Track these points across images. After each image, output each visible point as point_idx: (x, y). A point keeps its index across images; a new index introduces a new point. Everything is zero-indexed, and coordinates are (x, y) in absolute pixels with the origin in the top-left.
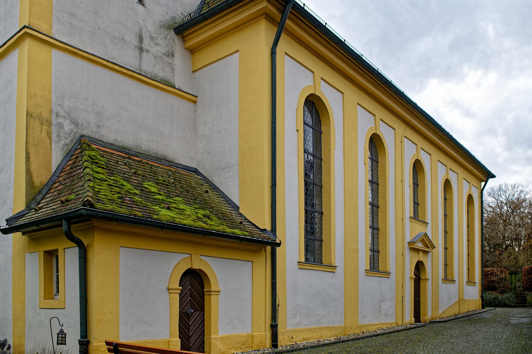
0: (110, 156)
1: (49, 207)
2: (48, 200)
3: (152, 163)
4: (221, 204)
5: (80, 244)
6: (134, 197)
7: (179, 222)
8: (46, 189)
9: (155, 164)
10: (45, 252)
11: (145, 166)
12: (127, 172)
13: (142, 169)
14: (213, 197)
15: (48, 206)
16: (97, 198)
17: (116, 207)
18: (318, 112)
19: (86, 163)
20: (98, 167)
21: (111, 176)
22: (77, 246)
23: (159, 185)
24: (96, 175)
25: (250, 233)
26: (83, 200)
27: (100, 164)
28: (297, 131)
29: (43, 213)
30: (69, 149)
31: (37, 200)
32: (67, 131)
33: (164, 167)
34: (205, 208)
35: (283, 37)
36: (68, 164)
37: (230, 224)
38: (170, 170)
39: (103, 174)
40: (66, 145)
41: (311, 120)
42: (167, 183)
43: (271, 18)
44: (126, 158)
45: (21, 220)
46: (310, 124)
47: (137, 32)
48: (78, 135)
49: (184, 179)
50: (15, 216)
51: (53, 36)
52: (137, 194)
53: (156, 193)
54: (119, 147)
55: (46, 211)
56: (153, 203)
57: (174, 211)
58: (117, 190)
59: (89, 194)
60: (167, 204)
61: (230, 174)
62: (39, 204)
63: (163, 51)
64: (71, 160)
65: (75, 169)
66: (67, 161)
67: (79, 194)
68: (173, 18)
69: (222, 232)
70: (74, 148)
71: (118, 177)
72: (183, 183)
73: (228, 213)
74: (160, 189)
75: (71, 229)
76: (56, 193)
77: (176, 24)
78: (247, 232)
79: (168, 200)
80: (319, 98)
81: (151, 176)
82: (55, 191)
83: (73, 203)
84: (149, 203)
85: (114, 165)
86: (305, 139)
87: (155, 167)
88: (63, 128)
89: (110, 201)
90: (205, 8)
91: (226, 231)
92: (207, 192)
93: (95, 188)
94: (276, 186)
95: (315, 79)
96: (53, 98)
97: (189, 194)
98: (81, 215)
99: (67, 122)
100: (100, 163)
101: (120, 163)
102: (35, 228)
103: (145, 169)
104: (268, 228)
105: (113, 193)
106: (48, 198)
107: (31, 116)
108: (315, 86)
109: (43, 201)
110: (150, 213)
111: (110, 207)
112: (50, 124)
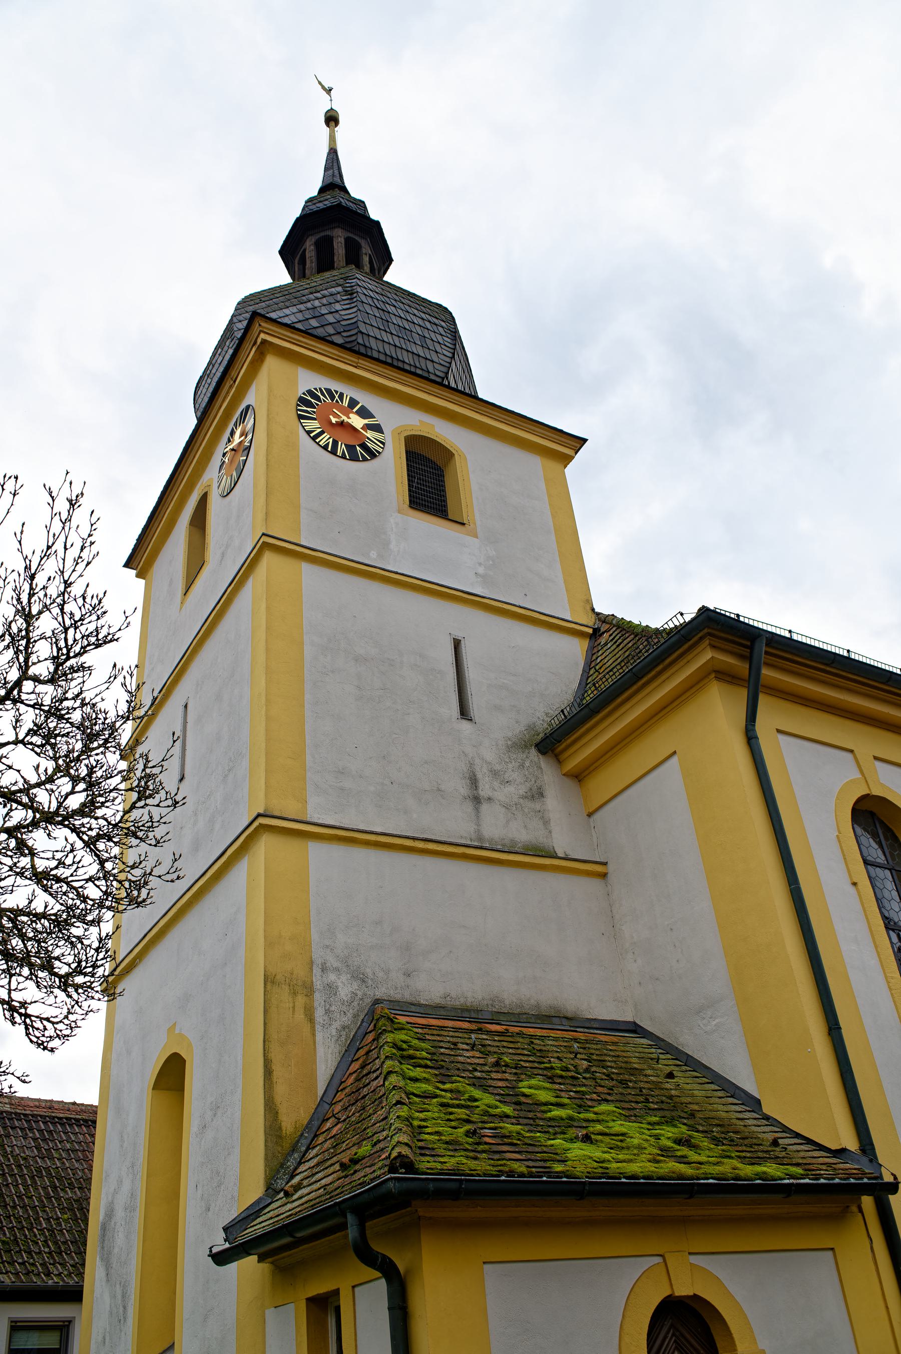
0: (438, 1035)
1: (316, 1182)
2: (312, 1165)
3: (531, 1031)
4: (712, 1100)
5: (389, 1271)
6: (502, 1125)
7: (618, 1171)
8: (306, 1137)
9: (539, 1033)
10: (310, 1301)
11: (518, 1042)
12: (478, 1064)
13: (510, 1051)
14: (688, 1087)
15: (314, 1179)
16: (420, 1144)
17: (465, 1161)
18: (890, 830)
19: (389, 1063)
20: (415, 1067)
21: (444, 1083)
22: (381, 1275)
23: (555, 1083)
24: (413, 1087)
25: (807, 1167)
26: (390, 1155)
27: (419, 1058)
28: (855, 884)
29: (304, 1200)
30: (351, 1037)
31: (288, 1168)
32: (344, 998)
33: (559, 1034)
34: (676, 1119)
35: (764, 701)
36: (351, 1069)
37: (748, 1152)
38: (575, 1040)
39: (426, 1080)
40: (344, 1028)
41: (880, 852)
42: (573, 1074)
43: (729, 675)
44: (472, 1031)
45: (255, 1223)
46: (878, 860)
47: (465, 770)
48: (368, 1001)
49: (611, 1053)
50: (243, 1216)
51: (309, 819)
52: (508, 1116)
53: (552, 1104)
54: (455, 1009)
55: (309, 1194)
56: (548, 1132)
57: (602, 1141)
58: (461, 1113)
59: (401, 1139)
60: (580, 1127)
61: (717, 1021)
62: (292, 1177)
63: (520, 791)
64: (357, 1060)
65: (366, 1080)
66: (349, 1063)
67: (379, 1141)
68: (531, 727)
69: (733, 1179)
70: (362, 1031)
71: (459, 1082)
72: (609, 1064)
73: (734, 1121)
74: (559, 1090)
75: (367, 1232)
76: (328, 1145)
77: (538, 735)
78: (798, 1165)
79: (582, 1116)
80: (883, 801)
81: (534, 1062)
82: (326, 1141)
83: (368, 1164)
84: (538, 1134)
85: (449, 1055)
86: (879, 896)
87: (538, 1039)
88: (335, 994)
89: (450, 1147)
90: (590, 692)
91: (742, 1173)
92: (671, 1075)
93: (413, 1119)
94: (840, 1028)
95: (861, 764)
96: (315, 936)
97: (629, 1091)
98: (389, 1195)
99: (344, 978)
100: (419, 1056)
101: (461, 1046)
102: (287, 1240)
103: (518, 1048)
104: (851, 1143)
105: (453, 1124)
106: (311, 1158)
107: (273, 982)
108: (865, 778)
109: (302, 1168)
110: (545, 1161)
111: (451, 1162)
112: (309, 990)
